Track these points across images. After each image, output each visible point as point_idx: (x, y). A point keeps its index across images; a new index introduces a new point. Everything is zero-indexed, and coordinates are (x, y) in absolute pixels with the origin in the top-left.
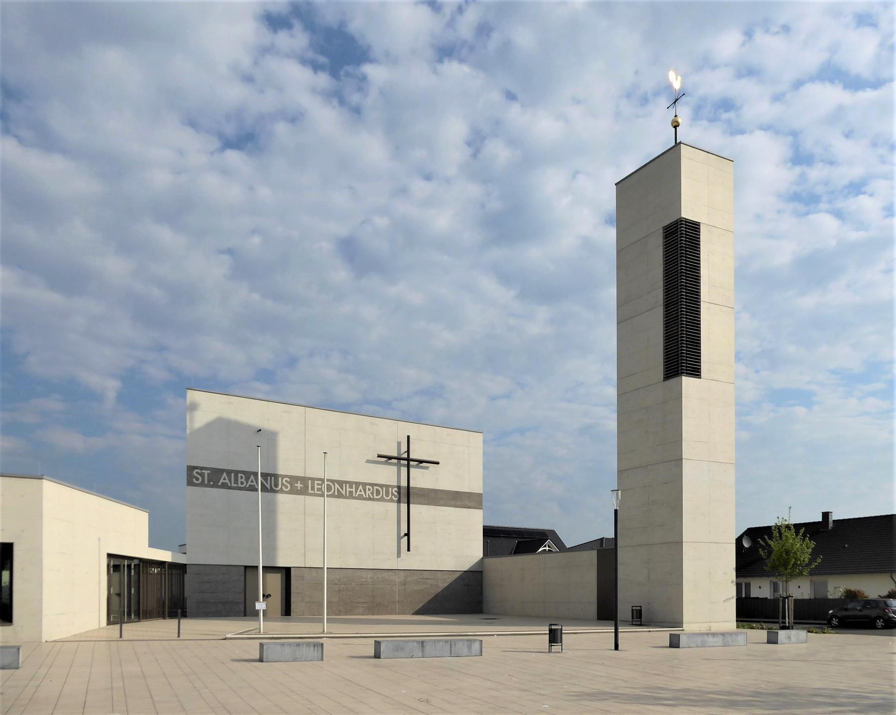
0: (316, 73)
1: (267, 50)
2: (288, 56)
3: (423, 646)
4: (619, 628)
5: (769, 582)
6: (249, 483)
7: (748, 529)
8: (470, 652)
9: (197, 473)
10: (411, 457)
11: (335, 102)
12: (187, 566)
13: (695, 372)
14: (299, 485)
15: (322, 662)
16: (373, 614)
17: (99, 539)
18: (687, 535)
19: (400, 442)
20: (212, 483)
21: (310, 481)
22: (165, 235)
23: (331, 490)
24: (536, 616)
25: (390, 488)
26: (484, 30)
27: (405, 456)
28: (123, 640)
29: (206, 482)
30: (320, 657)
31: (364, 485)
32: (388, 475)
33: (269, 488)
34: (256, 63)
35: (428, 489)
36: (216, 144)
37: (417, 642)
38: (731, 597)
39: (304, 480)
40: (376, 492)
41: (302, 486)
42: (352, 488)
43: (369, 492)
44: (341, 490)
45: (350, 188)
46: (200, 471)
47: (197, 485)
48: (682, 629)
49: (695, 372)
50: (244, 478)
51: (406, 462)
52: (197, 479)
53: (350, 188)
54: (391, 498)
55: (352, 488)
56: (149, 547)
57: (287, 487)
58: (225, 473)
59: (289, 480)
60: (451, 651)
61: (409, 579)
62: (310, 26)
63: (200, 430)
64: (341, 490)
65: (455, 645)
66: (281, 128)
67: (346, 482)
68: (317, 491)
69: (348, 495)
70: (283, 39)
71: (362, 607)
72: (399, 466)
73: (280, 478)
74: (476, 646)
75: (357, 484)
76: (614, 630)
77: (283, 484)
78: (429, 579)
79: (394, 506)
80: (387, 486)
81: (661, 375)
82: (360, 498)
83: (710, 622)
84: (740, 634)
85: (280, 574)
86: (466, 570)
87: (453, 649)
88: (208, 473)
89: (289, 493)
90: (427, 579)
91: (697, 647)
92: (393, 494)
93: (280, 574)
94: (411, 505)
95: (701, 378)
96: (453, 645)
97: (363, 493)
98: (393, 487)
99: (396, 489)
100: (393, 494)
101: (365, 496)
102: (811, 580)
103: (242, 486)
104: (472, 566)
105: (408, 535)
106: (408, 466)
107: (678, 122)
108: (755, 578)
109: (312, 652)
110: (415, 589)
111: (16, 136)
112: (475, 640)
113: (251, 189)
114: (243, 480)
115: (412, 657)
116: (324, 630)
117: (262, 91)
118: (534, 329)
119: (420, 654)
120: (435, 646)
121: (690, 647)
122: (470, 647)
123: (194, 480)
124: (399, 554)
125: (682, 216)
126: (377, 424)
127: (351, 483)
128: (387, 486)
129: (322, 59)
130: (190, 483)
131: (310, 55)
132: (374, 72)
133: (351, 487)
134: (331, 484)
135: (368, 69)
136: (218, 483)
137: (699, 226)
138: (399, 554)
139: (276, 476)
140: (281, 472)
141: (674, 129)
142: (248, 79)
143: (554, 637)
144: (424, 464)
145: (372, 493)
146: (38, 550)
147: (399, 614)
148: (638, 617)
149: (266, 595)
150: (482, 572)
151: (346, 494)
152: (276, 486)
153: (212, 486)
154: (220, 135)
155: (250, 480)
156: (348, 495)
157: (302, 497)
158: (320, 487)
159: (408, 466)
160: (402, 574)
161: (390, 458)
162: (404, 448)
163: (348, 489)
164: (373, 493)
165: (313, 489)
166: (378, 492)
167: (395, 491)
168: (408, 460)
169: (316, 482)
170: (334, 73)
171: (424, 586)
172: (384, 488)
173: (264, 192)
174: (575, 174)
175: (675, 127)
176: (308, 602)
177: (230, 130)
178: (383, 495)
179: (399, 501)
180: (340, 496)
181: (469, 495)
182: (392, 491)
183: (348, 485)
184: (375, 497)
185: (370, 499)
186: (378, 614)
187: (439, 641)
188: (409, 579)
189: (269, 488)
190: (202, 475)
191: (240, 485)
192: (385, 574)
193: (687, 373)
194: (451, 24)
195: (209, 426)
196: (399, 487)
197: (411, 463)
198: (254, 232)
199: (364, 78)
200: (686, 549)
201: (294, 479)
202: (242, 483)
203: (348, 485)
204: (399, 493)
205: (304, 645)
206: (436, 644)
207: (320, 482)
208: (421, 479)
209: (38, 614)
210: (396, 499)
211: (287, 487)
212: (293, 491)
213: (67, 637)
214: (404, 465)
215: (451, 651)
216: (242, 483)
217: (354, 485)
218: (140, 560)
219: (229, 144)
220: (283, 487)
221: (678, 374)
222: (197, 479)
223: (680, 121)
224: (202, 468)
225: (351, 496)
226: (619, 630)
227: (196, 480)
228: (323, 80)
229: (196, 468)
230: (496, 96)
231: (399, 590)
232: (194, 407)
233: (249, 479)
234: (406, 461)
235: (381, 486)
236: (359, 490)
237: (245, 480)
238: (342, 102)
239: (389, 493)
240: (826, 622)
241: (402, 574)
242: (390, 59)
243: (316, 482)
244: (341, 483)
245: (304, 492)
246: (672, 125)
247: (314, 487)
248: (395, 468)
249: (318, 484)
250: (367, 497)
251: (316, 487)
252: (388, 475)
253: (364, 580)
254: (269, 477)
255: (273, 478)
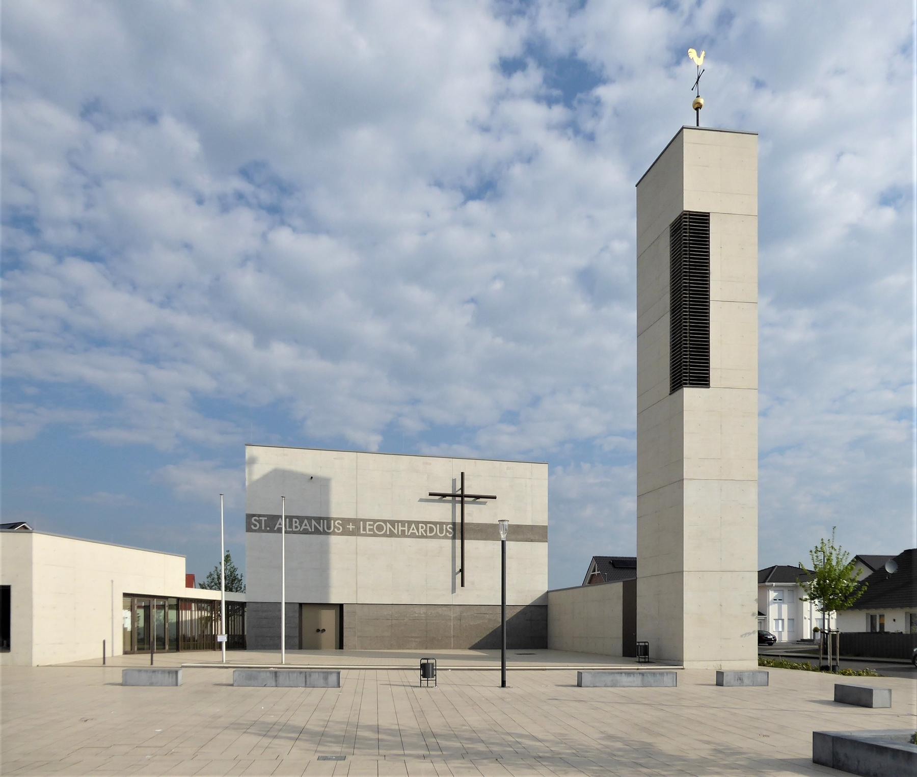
0: (550, 108)
1: (500, 97)
2: (524, 96)
3: (276, 676)
4: (507, 663)
5: (904, 615)
6: (303, 527)
7: (905, 551)
8: (327, 683)
9: (255, 520)
10: (466, 492)
11: (570, 132)
12: (247, 604)
13: (702, 380)
14: (351, 527)
15: (175, 688)
16: (426, 648)
17: (112, 581)
18: (689, 562)
19: (455, 479)
20: (268, 529)
21: (361, 522)
22: (416, 294)
23: (383, 530)
24: (582, 652)
25: (444, 526)
26: (725, 18)
27: (460, 492)
28: (105, 667)
29: (263, 528)
30: (175, 683)
31: (417, 523)
32: (443, 512)
33: (322, 531)
34: (493, 112)
35: (486, 524)
36: (460, 197)
37: (270, 672)
38: (751, 631)
39: (355, 521)
40: (429, 529)
41: (354, 527)
42: (405, 527)
43: (422, 530)
44: (393, 529)
45: (589, 217)
46: (257, 518)
47: (255, 531)
48: (682, 667)
49: (702, 380)
50: (298, 523)
51: (460, 499)
52: (255, 526)
53: (589, 217)
54: (446, 534)
55: (405, 527)
56: (186, 587)
57: (339, 529)
58: (413, 524)
59: (341, 522)
60: (306, 682)
61: (465, 614)
62: (543, 62)
63: (258, 481)
64: (393, 529)
65: (310, 676)
66: (517, 170)
67: (398, 522)
68: (369, 531)
69: (400, 534)
70: (518, 82)
71: (415, 641)
72: (454, 503)
73: (332, 521)
74: (333, 678)
75: (410, 523)
76: (501, 668)
77: (335, 527)
78: (487, 614)
79: (449, 542)
80: (441, 524)
81: (668, 390)
82: (413, 536)
83: (721, 660)
84: (667, 675)
85: (334, 611)
86: (528, 604)
87: (308, 680)
88: (265, 520)
89: (342, 534)
90: (485, 614)
91: (606, 686)
92: (447, 531)
93: (334, 611)
94: (466, 541)
95: (709, 387)
96: (308, 676)
97: (415, 531)
98: (447, 524)
99: (451, 526)
100: (447, 531)
101: (417, 534)
102: (867, 614)
103: (296, 530)
104: (535, 600)
105: (462, 570)
106: (462, 503)
107: (699, 103)
108: (889, 610)
109: (168, 679)
110: (472, 624)
111: (289, 226)
112: (331, 673)
113: (493, 236)
114: (297, 524)
115: (265, 686)
116: (223, 660)
117: (499, 139)
118: (794, 336)
119: (274, 684)
120: (289, 676)
121: (596, 687)
122: (326, 679)
123: (252, 526)
124: (454, 590)
125: (684, 209)
126: (430, 464)
127: (403, 523)
128: (441, 524)
129: (556, 93)
130: (249, 530)
131: (543, 91)
132: (608, 93)
133: (403, 526)
134: (384, 525)
135: (602, 92)
136: (274, 528)
137: (709, 216)
138: (454, 590)
139: (328, 519)
140: (333, 515)
141: (696, 111)
142: (485, 129)
143: (426, 671)
144: (481, 500)
145: (426, 531)
146: (29, 591)
147: (454, 648)
148: (642, 654)
149: (321, 630)
150: (547, 606)
151: (398, 533)
152: (329, 528)
153: (268, 532)
154: (463, 189)
155: (304, 524)
156: (400, 534)
157: (354, 537)
158: (372, 527)
159: (462, 503)
160: (458, 609)
161: (444, 495)
162: (459, 486)
163: (400, 528)
164: (427, 531)
165: (364, 529)
166: (431, 530)
167: (450, 528)
168: (462, 496)
169: (368, 523)
170: (567, 101)
171: (481, 621)
172: (438, 525)
173: (505, 237)
174: (840, 155)
175: (697, 109)
176: (360, 637)
177: (471, 182)
178: (437, 532)
179: (454, 538)
180: (392, 535)
181: (532, 528)
182: (446, 529)
183: (400, 524)
184: (428, 534)
185: (422, 537)
186: (432, 648)
187: (294, 672)
188: (465, 614)
189: (322, 531)
190: (260, 522)
191: (294, 530)
192: (440, 610)
193: (691, 384)
194: (690, 20)
195: (266, 477)
196: (454, 524)
197: (466, 499)
198: (495, 278)
199: (598, 102)
200: (687, 578)
201: (345, 521)
202: (296, 527)
203: (400, 524)
204: (454, 529)
205: (160, 672)
206: (290, 674)
207: (372, 523)
208: (475, 514)
209: (29, 643)
210: (451, 535)
211: (339, 529)
212: (346, 533)
213: (70, 663)
214: (458, 502)
215: (306, 682)
216: (296, 527)
217: (406, 524)
218: (178, 599)
219: (472, 195)
220: (336, 530)
221: (681, 385)
222: (255, 526)
223: (702, 101)
224: (259, 516)
225: (403, 535)
226: (506, 668)
227: (254, 526)
228: (558, 113)
229: (254, 515)
230: (744, 88)
231: (454, 625)
232: (253, 461)
233: (302, 523)
234: (460, 497)
235: (435, 523)
236: (412, 528)
237: (299, 524)
238: (577, 131)
239: (443, 530)
240: (910, 661)
241: (458, 609)
242: (625, 72)
243: (368, 523)
244: (393, 523)
245: (355, 533)
246: (694, 108)
247: (366, 528)
248: (449, 506)
249: (369, 525)
250: (420, 534)
251: (368, 527)
252: (443, 512)
253: (417, 615)
254: (322, 521)
255: (325, 521)
